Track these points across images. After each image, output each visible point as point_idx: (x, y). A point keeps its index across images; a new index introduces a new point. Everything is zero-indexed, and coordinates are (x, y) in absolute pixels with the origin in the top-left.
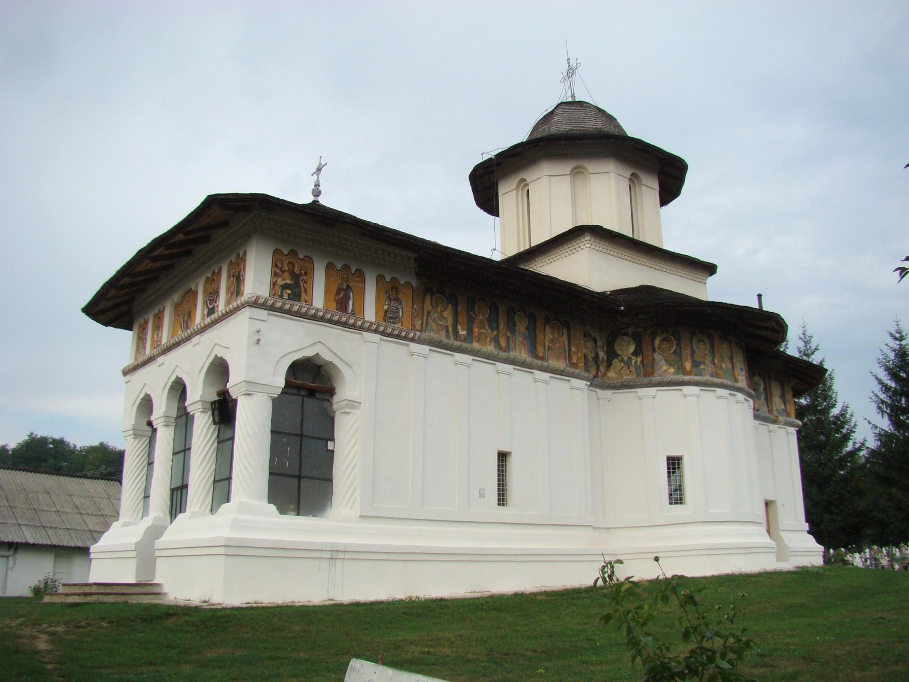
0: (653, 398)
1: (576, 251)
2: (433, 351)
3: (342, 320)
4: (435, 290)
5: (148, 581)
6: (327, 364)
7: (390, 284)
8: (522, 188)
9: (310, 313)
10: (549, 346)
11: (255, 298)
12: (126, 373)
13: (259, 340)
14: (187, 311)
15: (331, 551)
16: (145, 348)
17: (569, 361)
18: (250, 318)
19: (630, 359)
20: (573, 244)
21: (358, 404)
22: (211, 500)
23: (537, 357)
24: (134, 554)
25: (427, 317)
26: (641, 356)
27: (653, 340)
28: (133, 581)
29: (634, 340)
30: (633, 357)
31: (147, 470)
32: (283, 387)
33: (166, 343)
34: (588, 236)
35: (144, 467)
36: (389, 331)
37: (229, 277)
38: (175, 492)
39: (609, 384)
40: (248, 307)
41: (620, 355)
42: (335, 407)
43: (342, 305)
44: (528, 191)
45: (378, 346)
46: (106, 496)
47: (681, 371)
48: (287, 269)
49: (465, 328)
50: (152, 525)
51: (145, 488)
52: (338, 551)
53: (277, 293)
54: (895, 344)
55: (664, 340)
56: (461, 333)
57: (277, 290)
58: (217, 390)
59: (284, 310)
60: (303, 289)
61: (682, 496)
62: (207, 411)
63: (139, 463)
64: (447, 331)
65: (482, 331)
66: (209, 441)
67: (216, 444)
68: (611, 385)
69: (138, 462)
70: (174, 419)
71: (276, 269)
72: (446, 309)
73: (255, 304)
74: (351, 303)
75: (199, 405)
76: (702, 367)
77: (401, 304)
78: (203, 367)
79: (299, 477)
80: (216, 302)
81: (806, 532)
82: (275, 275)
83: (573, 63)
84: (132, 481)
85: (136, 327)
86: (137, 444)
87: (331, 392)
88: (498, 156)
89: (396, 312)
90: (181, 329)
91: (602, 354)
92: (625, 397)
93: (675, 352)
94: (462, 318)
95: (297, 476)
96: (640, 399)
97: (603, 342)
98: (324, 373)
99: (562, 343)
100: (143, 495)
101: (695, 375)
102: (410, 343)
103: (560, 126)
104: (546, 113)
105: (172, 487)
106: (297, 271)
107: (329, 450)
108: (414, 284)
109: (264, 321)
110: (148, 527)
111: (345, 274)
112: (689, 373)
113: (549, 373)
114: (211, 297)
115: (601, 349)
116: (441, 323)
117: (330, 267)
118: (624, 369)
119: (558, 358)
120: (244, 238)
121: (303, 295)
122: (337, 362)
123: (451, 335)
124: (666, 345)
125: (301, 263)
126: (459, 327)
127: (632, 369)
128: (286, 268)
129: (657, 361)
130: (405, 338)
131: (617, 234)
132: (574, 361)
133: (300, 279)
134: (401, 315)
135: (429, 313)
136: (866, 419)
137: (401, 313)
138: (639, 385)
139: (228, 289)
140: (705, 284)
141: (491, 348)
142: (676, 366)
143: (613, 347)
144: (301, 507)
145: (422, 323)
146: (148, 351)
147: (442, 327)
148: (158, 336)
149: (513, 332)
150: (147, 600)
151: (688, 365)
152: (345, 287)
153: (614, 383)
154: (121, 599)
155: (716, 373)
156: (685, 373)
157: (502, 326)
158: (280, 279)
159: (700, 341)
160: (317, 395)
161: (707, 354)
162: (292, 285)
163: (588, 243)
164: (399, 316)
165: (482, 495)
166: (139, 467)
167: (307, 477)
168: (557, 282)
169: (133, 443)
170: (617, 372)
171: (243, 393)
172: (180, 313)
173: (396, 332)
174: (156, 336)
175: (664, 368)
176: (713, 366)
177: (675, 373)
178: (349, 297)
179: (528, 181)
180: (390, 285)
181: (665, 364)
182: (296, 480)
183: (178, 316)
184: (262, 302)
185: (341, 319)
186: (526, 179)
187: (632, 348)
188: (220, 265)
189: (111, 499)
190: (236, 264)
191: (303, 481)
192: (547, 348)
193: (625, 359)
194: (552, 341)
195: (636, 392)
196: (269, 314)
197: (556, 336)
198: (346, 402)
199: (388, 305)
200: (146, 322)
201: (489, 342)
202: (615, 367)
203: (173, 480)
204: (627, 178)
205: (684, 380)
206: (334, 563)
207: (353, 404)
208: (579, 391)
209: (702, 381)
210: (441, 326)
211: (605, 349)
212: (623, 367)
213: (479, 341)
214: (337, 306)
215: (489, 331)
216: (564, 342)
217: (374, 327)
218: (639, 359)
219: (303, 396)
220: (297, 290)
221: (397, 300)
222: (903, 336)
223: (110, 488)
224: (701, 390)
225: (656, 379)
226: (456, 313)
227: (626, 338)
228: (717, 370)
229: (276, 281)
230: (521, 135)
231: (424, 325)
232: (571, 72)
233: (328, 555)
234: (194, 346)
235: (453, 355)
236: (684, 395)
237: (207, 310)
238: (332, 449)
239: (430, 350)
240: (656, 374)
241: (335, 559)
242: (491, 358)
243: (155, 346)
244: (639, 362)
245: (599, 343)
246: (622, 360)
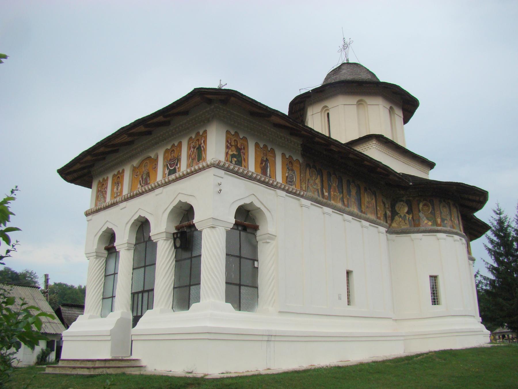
0: (421, 240)
1: (365, 150)
2: (334, 212)
3: (266, 181)
4: (311, 165)
5: (125, 357)
6: (253, 210)
7: (288, 160)
8: (324, 113)
9: (248, 174)
10: (367, 206)
11: (218, 161)
12: (87, 214)
13: (220, 190)
14: (145, 172)
15: (268, 335)
16: (105, 198)
17: (377, 215)
18: (214, 175)
19: (405, 216)
20: (364, 146)
21: (273, 237)
22: (172, 301)
23: (362, 212)
24: (109, 338)
25: (308, 183)
26: (412, 214)
27: (418, 205)
28: (109, 357)
29: (407, 204)
30: (407, 215)
31: (105, 279)
32: (234, 223)
33: (127, 194)
34: (374, 141)
35: (102, 278)
36: (291, 190)
37: (189, 148)
38: (136, 296)
39: (394, 231)
40: (213, 167)
41: (399, 214)
42: (258, 238)
43: (264, 171)
44: (328, 114)
45: (285, 199)
46: (32, 298)
47: (435, 225)
48: (234, 144)
49: (327, 191)
50: (120, 318)
51: (103, 292)
52: (271, 335)
53: (228, 159)
54: (497, 217)
55: (424, 205)
56: (325, 194)
57: (229, 158)
58: (176, 225)
59: (234, 171)
60: (243, 159)
61: (433, 293)
62: (169, 239)
63: (99, 276)
64: (318, 192)
65: (335, 193)
66: (170, 260)
67: (174, 262)
68: (395, 231)
69: (99, 274)
70: (133, 245)
71: (227, 143)
72: (317, 178)
73: (217, 166)
74: (268, 170)
75: (164, 235)
76: (446, 222)
77: (294, 173)
78: (166, 209)
79: (240, 285)
80: (177, 165)
81: (480, 323)
82: (227, 147)
83: (347, 41)
84: (94, 287)
85: (95, 185)
86: (98, 262)
87: (256, 228)
88: (313, 90)
89: (292, 178)
90: (140, 184)
91: (389, 213)
92: (404, 239)
93: (431, 213)
94: (325, 184)
95: (238, 284)
96: (413, 240)
97: (389, 205)
98: (251, 216)
99: (372, 204)
100: (102, 297)
101: (443, 227)
102: (301, 198)
103: (346, 75)
104: (333, 69)
105: (133, 292)
106: (239, 146)
107: (255, 267)
108: (301, 161)
109: (222, 178)
110: (118, 319)
111: (265, 151)
112: (440, 225)
114: (171, 162)
115: (387, 209)
116: (315, 187)
117: (257, 145)
118: (401, 222)
119: (371, 213)
120: (207, 121)
121: (243, 162)
122: (262, 208)
123: (321, 196)
124: (426, 208)
125: (241, 141)
126: (324, 190)
127: (407, 222)
128: (233, 144)
129: (421, 218)
130: (298, 195)
131: (390, 141)
132: (379, 216)
133: (241, 151)
134: (294, 180)
135: (308, 180)
136: (482, 259)
137: (294, 178)
138: (413, 232)
139: (189, 156)
140: (428, 174)
141: (340, 205)
142: (432, 221)
143: (395, 208)
144: (241, 306)
145: (306, 186)
146: (109, 200)
147: (316, 190)
148: (117, 189)
149: (350, 195)
150: (134, 371)
151: (439, 221)
152: (265, 160)
153: (397, 230)
154: (119, 371)
155: (453, 226)
156: (437, 225)
157: (345, 191)
158: (230, 150)
159: (444, 206)
160: (248, 230)
161: (448, 214)
162: (237, 155)
163: (374, 145)
164: (293, 180)
165: (340, 298)
166: (99, 278)
167: (244, 286)
168: (381, 165)
169: (95, 261)
170: (398, 223)
171: (210, 226)
172: (139, 173)
173: (294, 191)
174: (115, 190)
175: (426, 222)
176: (451, 222)
177: (432, 225)
178: (268, 166)
180: (289, 160)
181: (426, 219)
182: (238, 287)
183: (136, 176)
184: (222, 165)
185: (265, 180)
187: (406, 209)
188: (180, 141)
189: (35, 300)
190: (195, 140)
191: (242, 287)
192: (366, 207)
193: (402, 216)
194: (368, 202)
196: (225, 174)
197: (370, 200)
198: (269, 235)
199: (288, 173)
200: (106, 181)
201: (339, 201)
202: (396, 220)
203: (133, 287)
205: (438, 229)
206: (269, 343)
207: (272, 237)
209: (448, 230)
210: (315, 189)
211: (390, 209)
212: (401, 221)
213: (334, 200)
214: (261, 171)
215: (339, 194)
216: (373, 204)
217: (283, 186)
218: (411, 216)
219: (240, 231)
220: (239, 159)
221: (292, 170)
222: (501, 212)
223: (34, 293)
224: (447, 236)
225: (422, 228)
226: (322, 181)
227: (402, 203)
228: (453, 224)
229: (228, 151)
230: (318, 82)
231: (307, 187)
232: (346, 46)
233: (266, 338)
234: (156, 195)
235: (322, 208)
237: (168, 171)
238: (257, 267)
239: (286, 195)
240: (421, 226)
241: (270, 341)
242: (341, 211)
243: (115, 196)
244: (410, 218)
245: (387, 206)
246: (400, 217)
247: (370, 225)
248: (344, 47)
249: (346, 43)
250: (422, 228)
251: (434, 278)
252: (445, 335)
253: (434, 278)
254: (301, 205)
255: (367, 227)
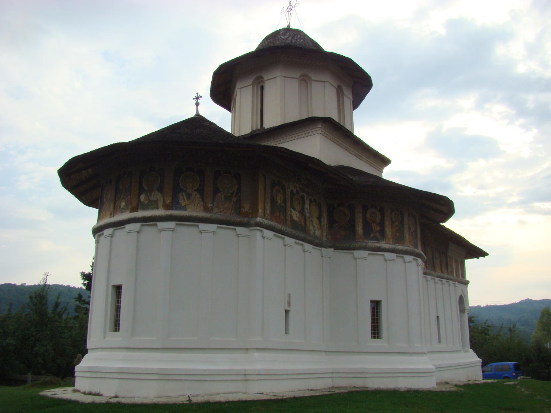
2: (372, 254)
44: (262, 88)
61: (373, 329)
96: (356, 259)
113: (368, 250)
163: (319, 130)
179: (265, 79)
186: (264, 77)
195: (353, 253)
196: (313, 248)
204: (240, 91)
208: (308, 253)
230: (252, 46)
236: (200, 231)
239: (397, 256)
247: (296, 243)
248: (291, 8)
249: (291, 4)
250: (405, 245)
251: (376, 305)
252: (295, 377)
253: (376, 305)
254: (262, 237)
255: (269, 239)
